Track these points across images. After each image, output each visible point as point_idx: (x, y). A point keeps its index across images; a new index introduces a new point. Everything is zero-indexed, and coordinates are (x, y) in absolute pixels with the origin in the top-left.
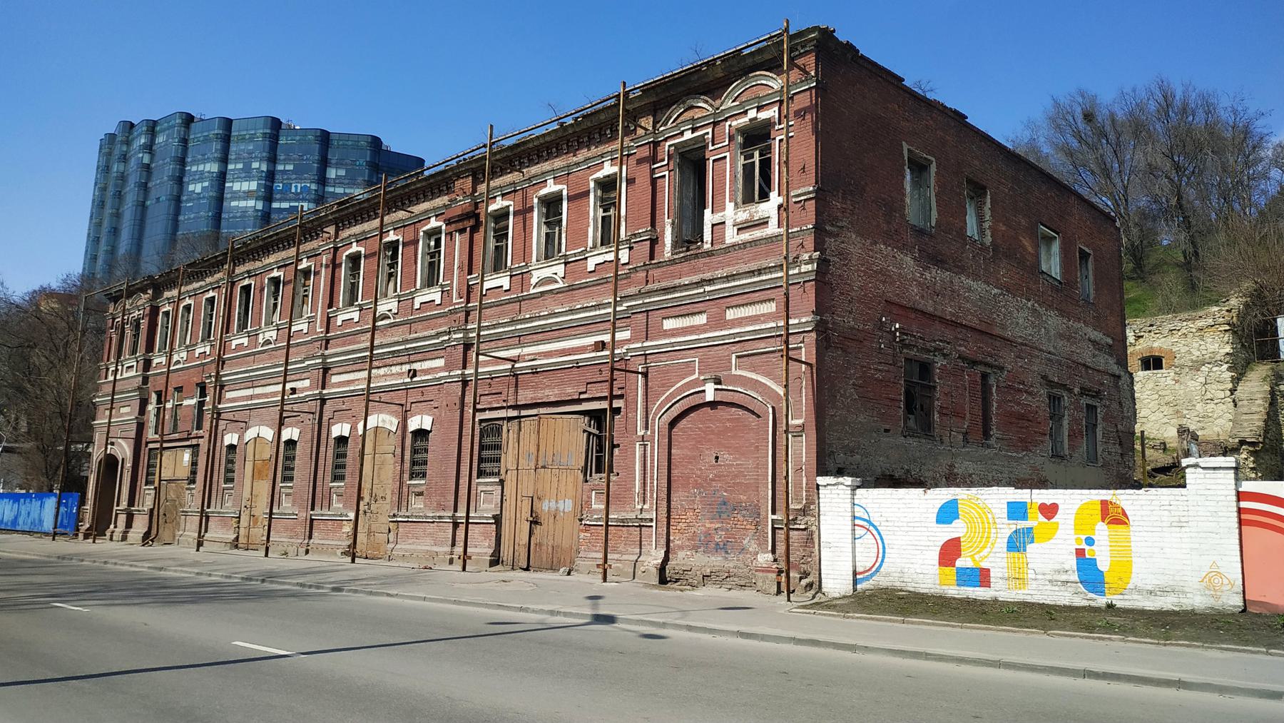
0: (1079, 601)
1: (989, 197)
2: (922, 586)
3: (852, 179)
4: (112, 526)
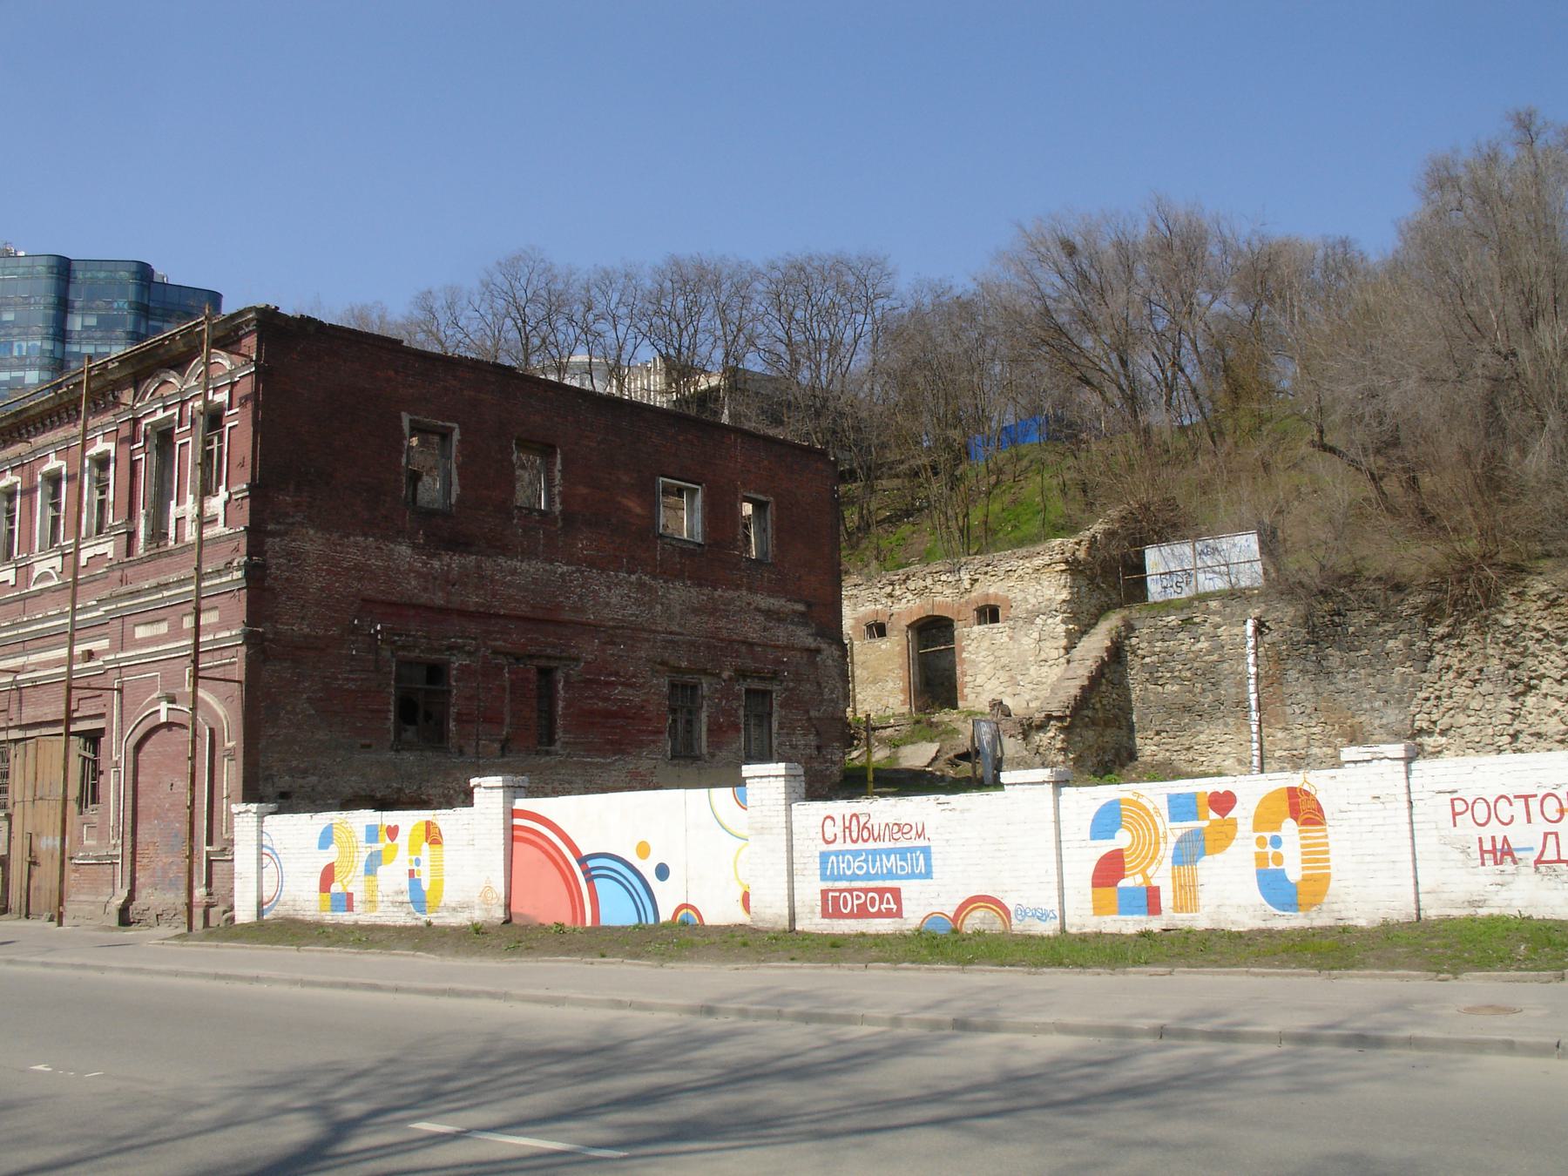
0: (411, 922)
1: (559, 461)
2: (309, 913)
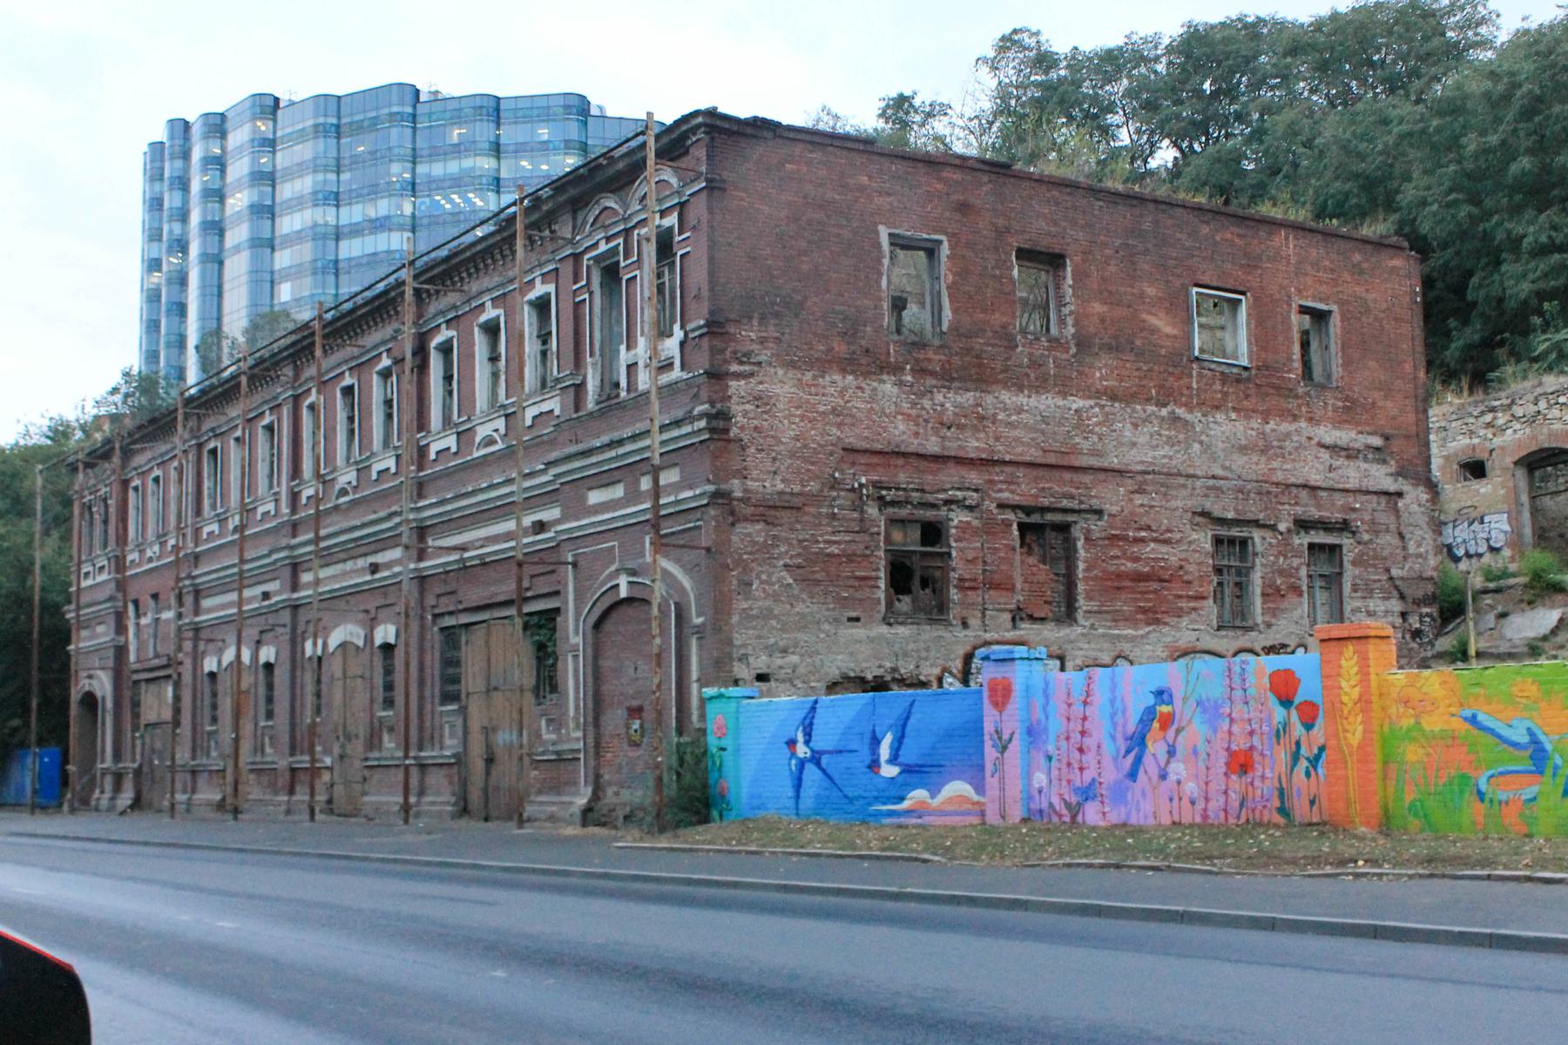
3: (776, 295)
4: (97, 791)
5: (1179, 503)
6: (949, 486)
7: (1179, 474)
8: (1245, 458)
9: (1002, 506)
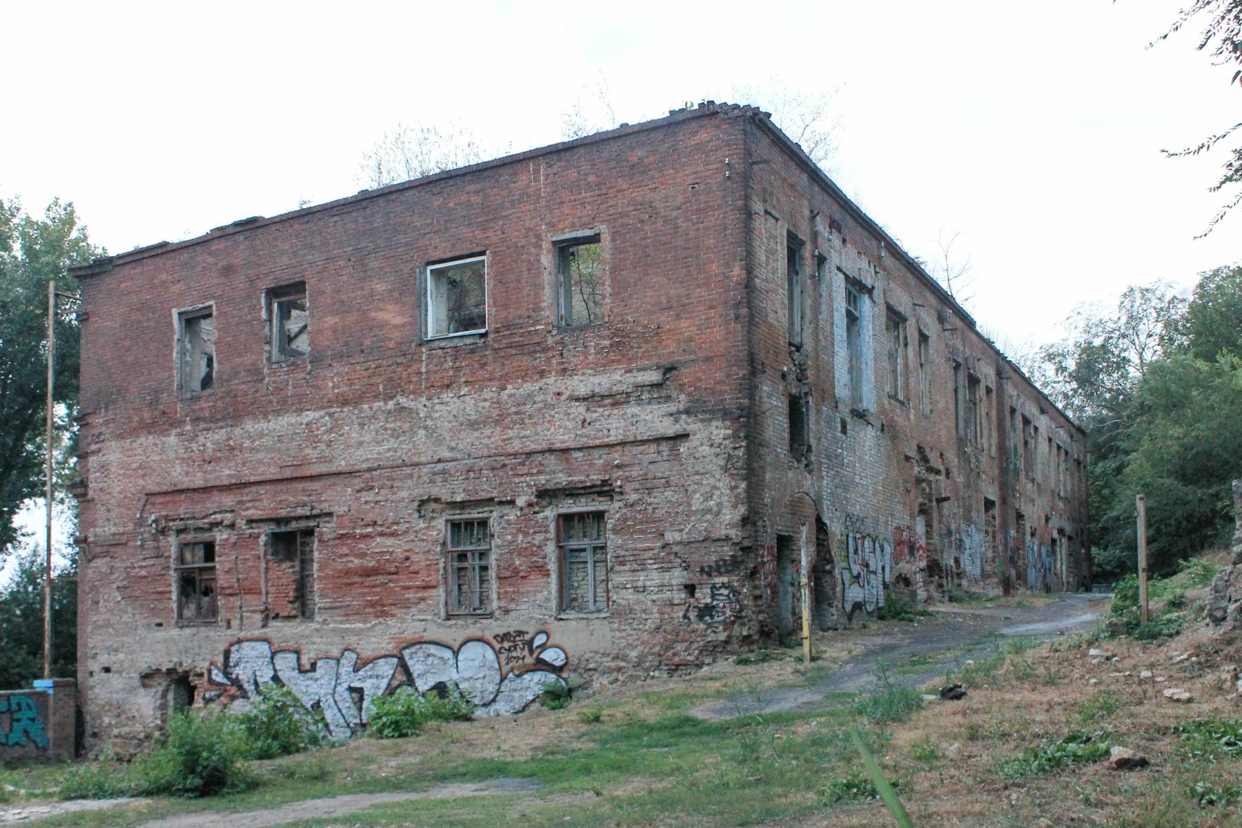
5: (404, 494)
6: (211, 511)
7: (404, 464)
8: (477, 434)
9: (250, 522)
